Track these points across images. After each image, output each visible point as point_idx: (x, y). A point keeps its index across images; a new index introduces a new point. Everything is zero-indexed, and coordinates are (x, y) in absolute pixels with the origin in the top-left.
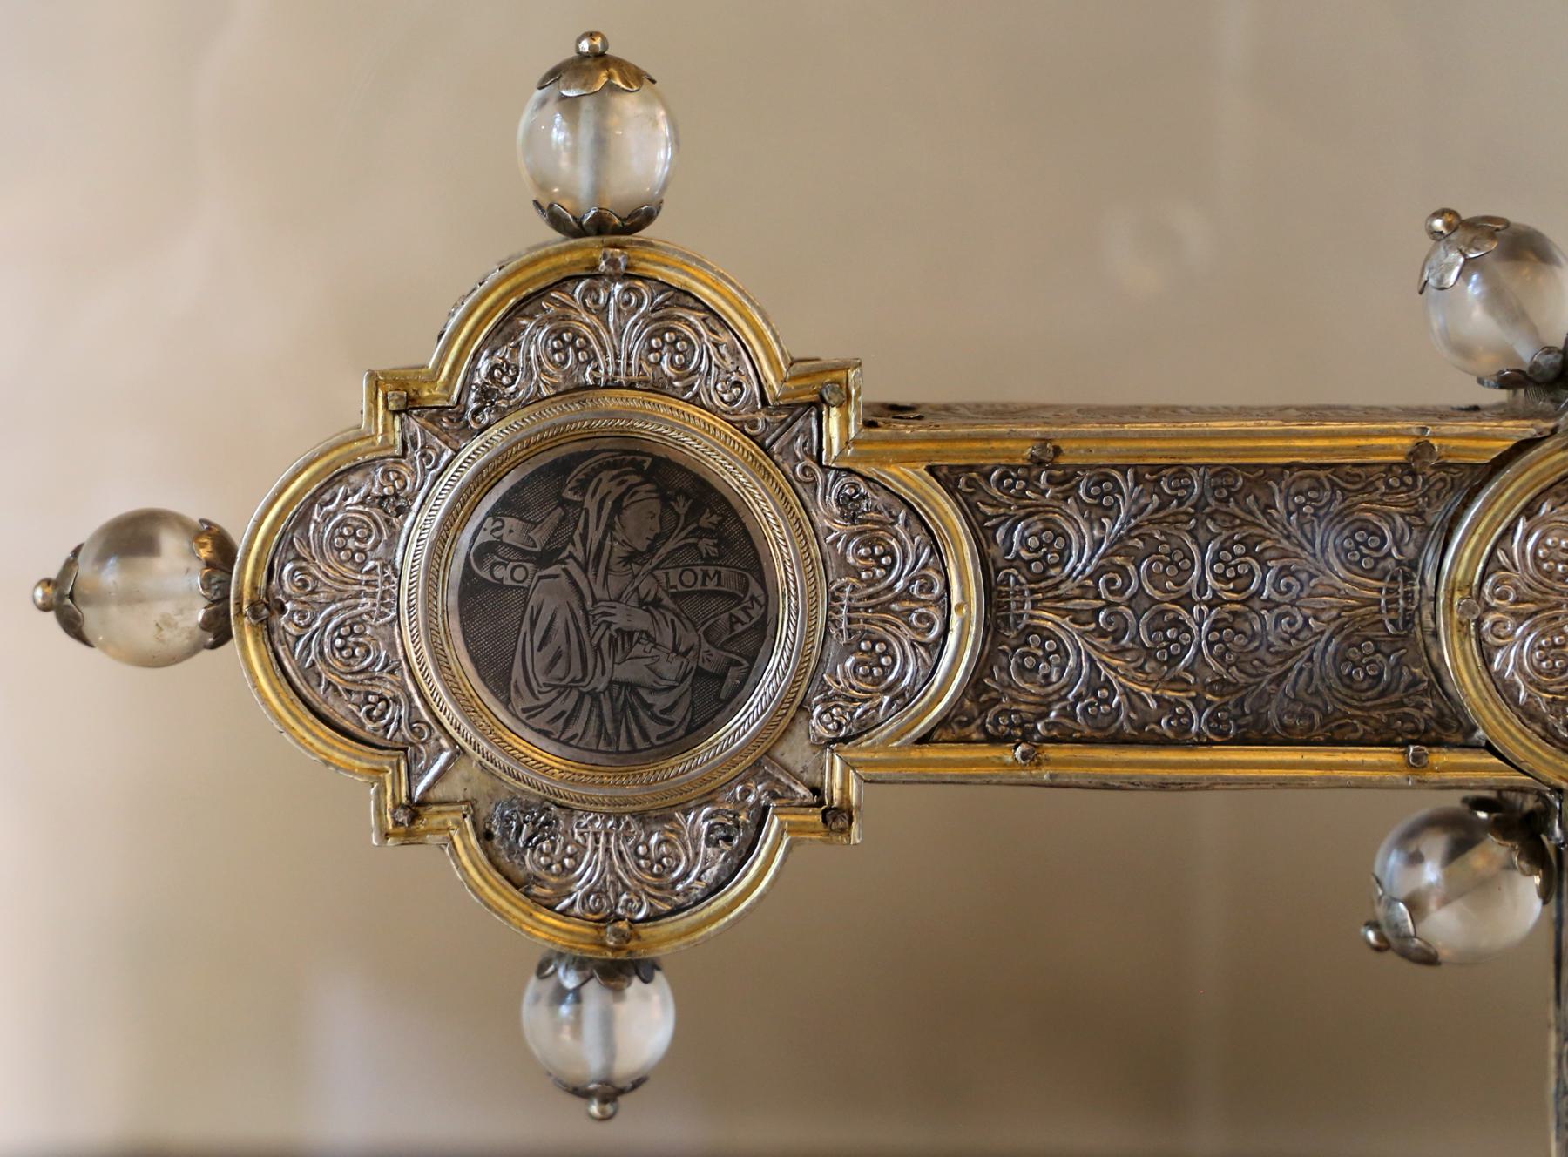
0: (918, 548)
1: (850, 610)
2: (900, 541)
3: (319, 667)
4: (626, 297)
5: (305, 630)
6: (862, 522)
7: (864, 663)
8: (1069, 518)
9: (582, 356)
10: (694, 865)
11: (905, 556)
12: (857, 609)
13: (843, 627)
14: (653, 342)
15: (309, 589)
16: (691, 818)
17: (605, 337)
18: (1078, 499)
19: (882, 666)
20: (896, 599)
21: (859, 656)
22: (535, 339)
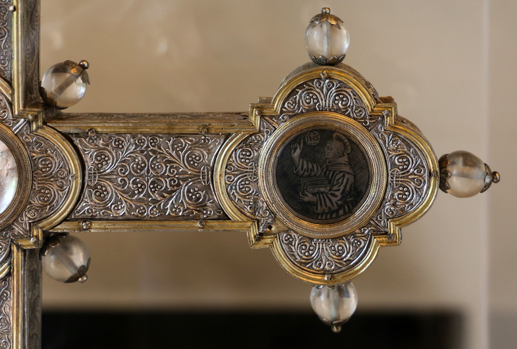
0: (416, 159)
1: (396, 178)
2: (411, 158)
3: (235, 194)
4: (329, 84)
6: (399, 151)
7: (400, 194)
8: (110, 152)
9: (316, 101)
11: (413, 161)
12: (398, 178)
13: (36, 185)
14: (337, 97)
15: (232, 170)
17: (322, 96)
18: (112, 146)
19: (406, 195)
20: (411, 174)
21: (399, 192)
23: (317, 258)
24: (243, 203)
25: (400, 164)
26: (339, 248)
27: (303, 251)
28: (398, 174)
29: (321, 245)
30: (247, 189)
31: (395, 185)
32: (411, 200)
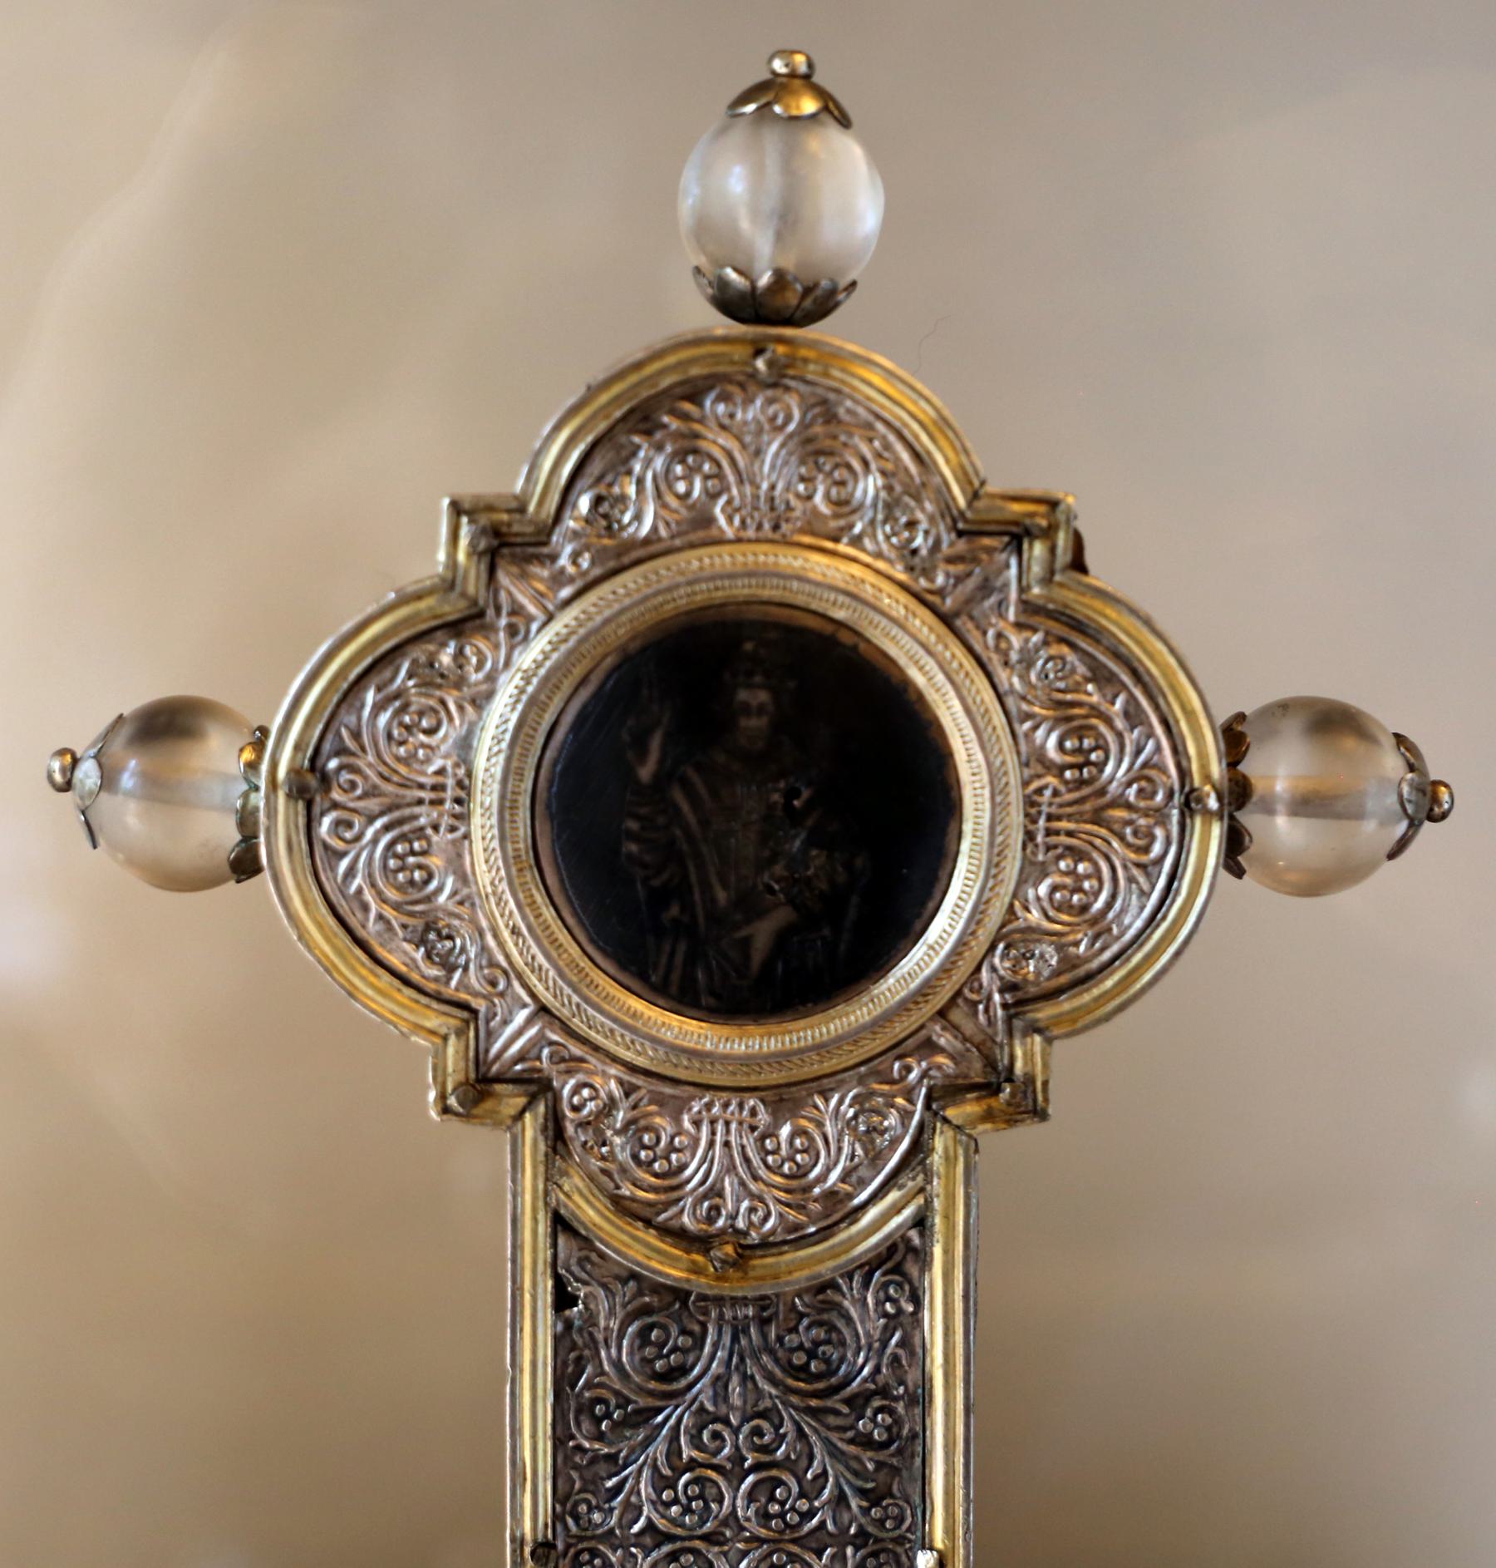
1: (1050, 818)
3: (368, 896)
5: (352, 846)
10: (836, 1163)
16: (833, 1102)
22: (649, 462)
23: (703, 1182)
24: (400, 933)
25: (1069, 759)
26: (798, 1142)
27: (643, 1154)
28: (1058, 800)
29: (720, 1127)
30: (417, 875)
31: (1042, 849)
32: (1109, 905)
